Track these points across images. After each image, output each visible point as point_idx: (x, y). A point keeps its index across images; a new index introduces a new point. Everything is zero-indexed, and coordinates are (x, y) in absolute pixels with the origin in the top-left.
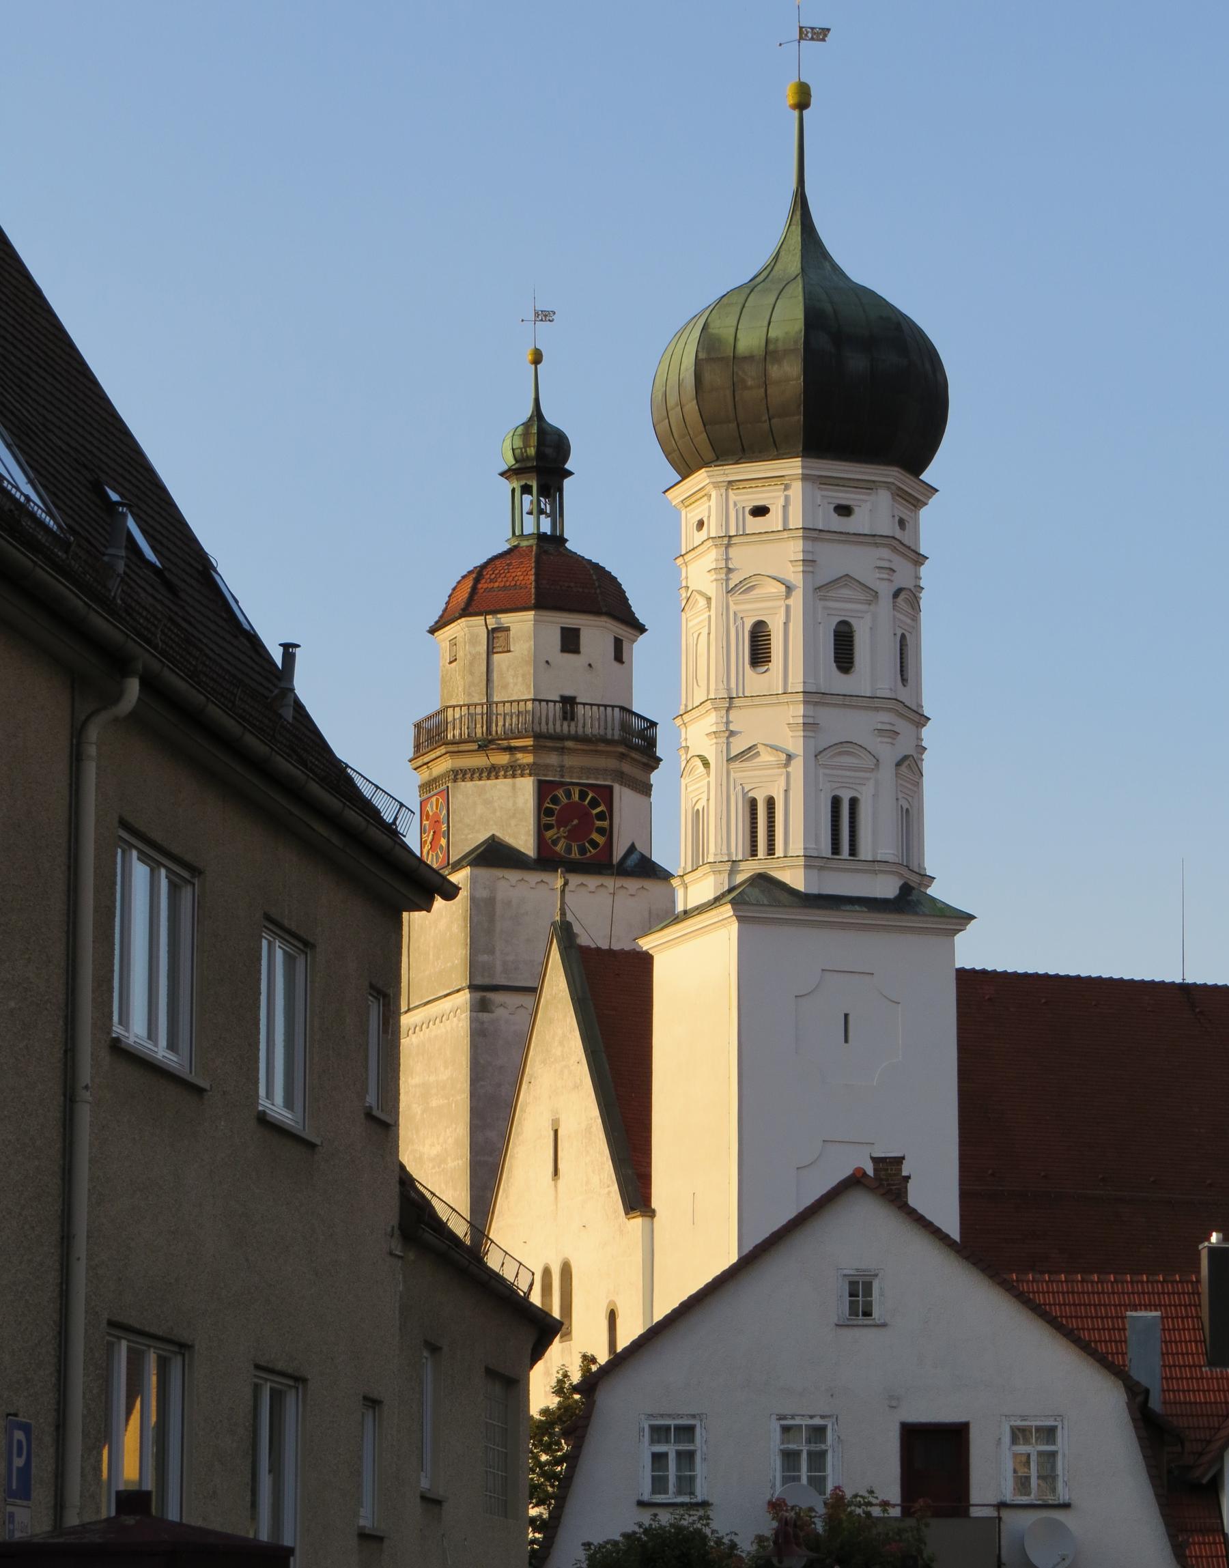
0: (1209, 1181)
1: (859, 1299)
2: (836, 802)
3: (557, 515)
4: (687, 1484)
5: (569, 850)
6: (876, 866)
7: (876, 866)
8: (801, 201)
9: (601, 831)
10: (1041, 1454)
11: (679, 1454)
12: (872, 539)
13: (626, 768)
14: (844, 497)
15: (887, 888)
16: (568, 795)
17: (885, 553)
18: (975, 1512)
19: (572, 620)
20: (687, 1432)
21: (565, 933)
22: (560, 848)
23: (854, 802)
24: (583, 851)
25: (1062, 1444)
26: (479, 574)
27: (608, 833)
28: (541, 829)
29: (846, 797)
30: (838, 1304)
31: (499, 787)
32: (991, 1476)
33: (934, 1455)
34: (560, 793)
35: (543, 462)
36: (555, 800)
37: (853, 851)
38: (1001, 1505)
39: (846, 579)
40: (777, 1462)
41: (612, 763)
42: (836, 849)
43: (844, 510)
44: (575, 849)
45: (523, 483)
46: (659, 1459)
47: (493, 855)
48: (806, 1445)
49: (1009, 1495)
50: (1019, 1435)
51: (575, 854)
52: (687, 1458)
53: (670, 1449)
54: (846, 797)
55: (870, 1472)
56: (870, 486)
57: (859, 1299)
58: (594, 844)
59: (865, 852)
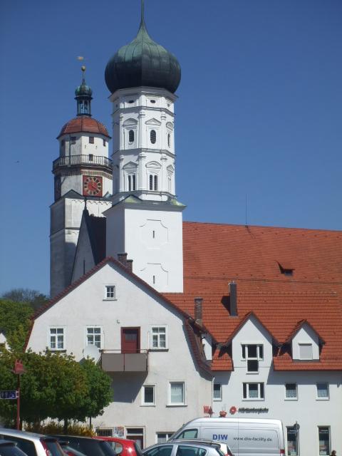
0: (84, 67)
1: (111, 290)
2: (151, 177)
5: (91, 193)
7: (161, 194)
9: (99, 188)
10: (161, 336)
11: (59, 337)
12: (161, 110)
15: (165, 198)
16: (91, 179)
17: (164, 113)
18: (141, 352)
19: (91, 135)
20: (61, 331)
21: (86, 212)
22: (89, 193)
23: (156, 177)
24: (94, 193)
25: (167, 333)
27: (101, 189)
28: (84, 187)
29: (153, 175)
30: (117, 292)
32: (146, 342)
33: (131, 335)
34: (88, 178)
36: (87, 180)
37: (156, 188)
38: (150, 350)
42: (151, 188)
43: (153, 102)
44: (89, 191)
48: (94, 335)
49: (152, 348)
50: (155, 330)
51: (93, 195)
52: (61, 338)
53: (56, 335)
54: (153, 175)
55: (112, 342)
57: (111, 290)
58: (98, 191)
59: (160, 189)
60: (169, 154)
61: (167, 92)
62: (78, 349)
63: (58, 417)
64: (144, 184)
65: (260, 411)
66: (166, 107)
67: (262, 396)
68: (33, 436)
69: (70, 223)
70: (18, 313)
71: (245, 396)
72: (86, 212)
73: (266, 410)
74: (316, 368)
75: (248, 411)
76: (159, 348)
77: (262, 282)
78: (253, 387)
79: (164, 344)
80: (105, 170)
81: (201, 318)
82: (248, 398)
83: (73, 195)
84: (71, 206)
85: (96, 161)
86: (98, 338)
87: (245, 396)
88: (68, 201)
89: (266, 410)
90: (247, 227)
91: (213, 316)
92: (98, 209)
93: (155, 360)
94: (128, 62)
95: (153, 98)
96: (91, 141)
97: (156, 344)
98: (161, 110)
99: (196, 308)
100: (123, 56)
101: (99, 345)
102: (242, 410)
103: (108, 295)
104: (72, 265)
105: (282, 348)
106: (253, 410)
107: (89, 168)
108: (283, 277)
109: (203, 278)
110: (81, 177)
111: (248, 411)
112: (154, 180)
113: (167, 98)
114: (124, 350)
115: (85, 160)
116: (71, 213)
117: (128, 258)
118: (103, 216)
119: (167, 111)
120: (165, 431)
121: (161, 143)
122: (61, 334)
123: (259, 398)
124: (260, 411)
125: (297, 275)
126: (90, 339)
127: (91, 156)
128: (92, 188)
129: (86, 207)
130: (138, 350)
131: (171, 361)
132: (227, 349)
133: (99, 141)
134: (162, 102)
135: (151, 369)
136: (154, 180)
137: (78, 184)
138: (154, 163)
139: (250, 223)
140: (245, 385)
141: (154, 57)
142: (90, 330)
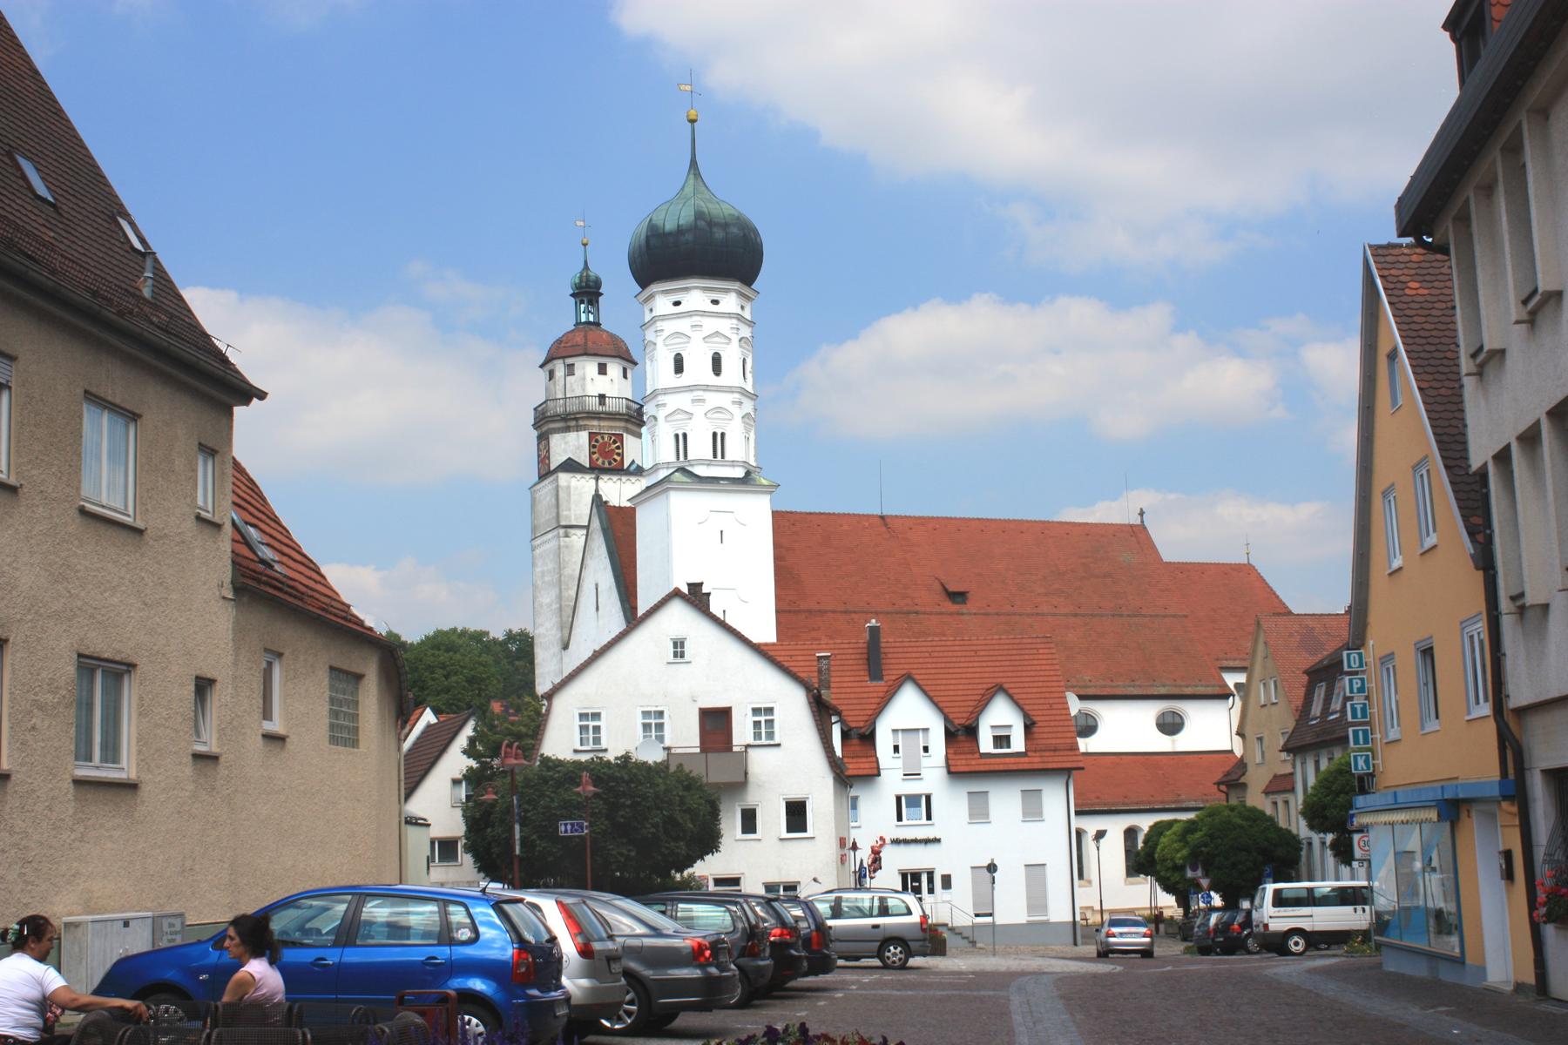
1: (679, 647)
3: (597, 314)
4: (597, 741)
6: (733, 464)
7: (733, 464)
8: (694, 164)
12: (729, 315)
13: (630, 426)
14: (715, 296)
15: (739, 473)
19: (603, 360)
20: (770, 711)
21: (597, 498)
25: (776, 717)
26: (559, 341)
27: (621, 455)
28: (591, 454)
30: (689, 649)
31: (572, 436)
32: (742, 732)
33: (716, 722)
35: (588, 291)
38: (748, 746)
39: (717, 333)
40: (640, 729)
41: (622, 424)
42: (715, 456)
43: (715, 302)
45: (1126, 826)
46: (757, 724)
47: (570, 466)
48: (654, 723)
49: (751, 740)
50: (756, 711)
52: (770, 723)
53: (762, 719)
55: (684, 735)
56: (727, 291)
57: (679, 647)
59: (728, 457)
60: (744, 392)
61: (737, 285)
62: (622, 739)
63: (65, 1041)
64: (700, 448)
65: (927, 841)
66: (739, 311)
67: (929, 817)
68: (538, 895)
69: (568, 517)
70: (1071, 688)
71: (900, 818)
72: (597, 498)
73: (937, 841)
74: (1021, 767)
75: (906, 842)
76: (764, 741)
77: (912, 616)
78: (913, 800)
79: (770, 735)
80: (627, 421)
81: (829, 688)
82: (905, 821)
83: (570, 466)
84: (568, 487)
85: (611, 405)
86: (660, 727)
87: (900, 818)
88: (564, 478)
89: (937, 841)
90: (882, 517)
91: (846, 688)
92: (618, 491)
93: (761, 763)
94: (670, 234)
95: (715, 296)
96: (602, 370)
97: (757, 736)
98: (729, 315)
99: (820, 671)
100: (660, 223)
101: (661, 739)
102: (896, 842)
103: (675, 655)
104: (573, 593)
105: (961, 734)
106: (915, 841)
107: (600, 419)
108: (950, 607)
109: (809, 611)
110: (584, 435)
111: (906, 842)
112: (718, 440)
113: (741, 295)
114: (705, 746)
115: (593, 404)
116: (569, 501)
117: (705, 590)
118: (628, 504)
119: (740, 318)
120: (777, 880)
121: (732, 372)
122: (596, 723)
123: (924, 820)
124: (927, 841)
125: (971, 606)
126: (646, 727)
127: (602, 397)
128: (606, 454)
129: (597, 490)
130: (730, 749)
131: (790, 761)
132: (869, 738)
133: (614, 369)
134: (730, 302)
135: (751, 778)
136: (718, 440)
137: (579, 447)
138: (719, 409)
139: (888, 511)
140: (899, 799)
141: (717, 224)
142: (646, 714)
